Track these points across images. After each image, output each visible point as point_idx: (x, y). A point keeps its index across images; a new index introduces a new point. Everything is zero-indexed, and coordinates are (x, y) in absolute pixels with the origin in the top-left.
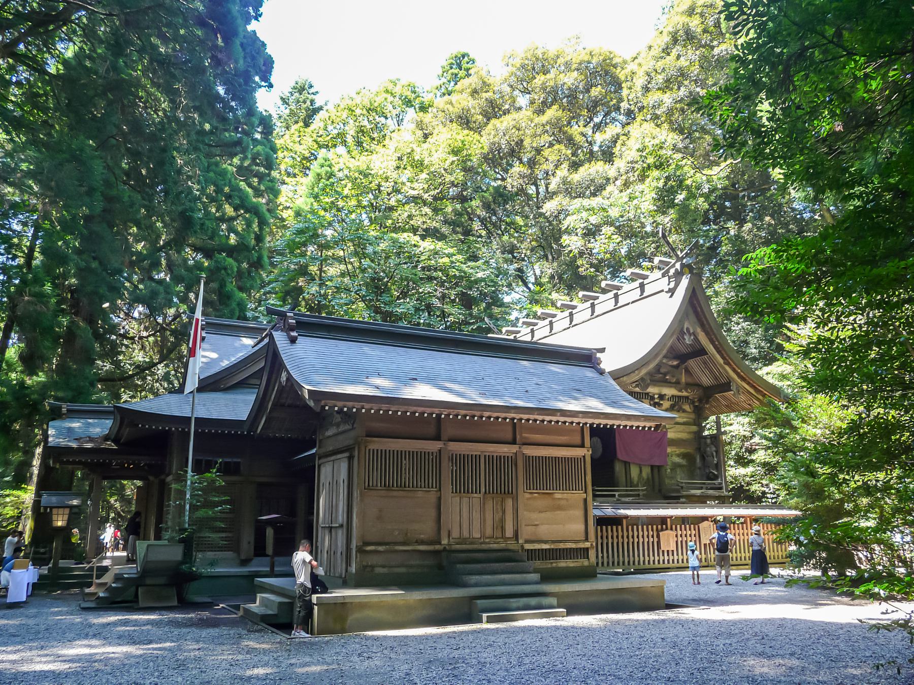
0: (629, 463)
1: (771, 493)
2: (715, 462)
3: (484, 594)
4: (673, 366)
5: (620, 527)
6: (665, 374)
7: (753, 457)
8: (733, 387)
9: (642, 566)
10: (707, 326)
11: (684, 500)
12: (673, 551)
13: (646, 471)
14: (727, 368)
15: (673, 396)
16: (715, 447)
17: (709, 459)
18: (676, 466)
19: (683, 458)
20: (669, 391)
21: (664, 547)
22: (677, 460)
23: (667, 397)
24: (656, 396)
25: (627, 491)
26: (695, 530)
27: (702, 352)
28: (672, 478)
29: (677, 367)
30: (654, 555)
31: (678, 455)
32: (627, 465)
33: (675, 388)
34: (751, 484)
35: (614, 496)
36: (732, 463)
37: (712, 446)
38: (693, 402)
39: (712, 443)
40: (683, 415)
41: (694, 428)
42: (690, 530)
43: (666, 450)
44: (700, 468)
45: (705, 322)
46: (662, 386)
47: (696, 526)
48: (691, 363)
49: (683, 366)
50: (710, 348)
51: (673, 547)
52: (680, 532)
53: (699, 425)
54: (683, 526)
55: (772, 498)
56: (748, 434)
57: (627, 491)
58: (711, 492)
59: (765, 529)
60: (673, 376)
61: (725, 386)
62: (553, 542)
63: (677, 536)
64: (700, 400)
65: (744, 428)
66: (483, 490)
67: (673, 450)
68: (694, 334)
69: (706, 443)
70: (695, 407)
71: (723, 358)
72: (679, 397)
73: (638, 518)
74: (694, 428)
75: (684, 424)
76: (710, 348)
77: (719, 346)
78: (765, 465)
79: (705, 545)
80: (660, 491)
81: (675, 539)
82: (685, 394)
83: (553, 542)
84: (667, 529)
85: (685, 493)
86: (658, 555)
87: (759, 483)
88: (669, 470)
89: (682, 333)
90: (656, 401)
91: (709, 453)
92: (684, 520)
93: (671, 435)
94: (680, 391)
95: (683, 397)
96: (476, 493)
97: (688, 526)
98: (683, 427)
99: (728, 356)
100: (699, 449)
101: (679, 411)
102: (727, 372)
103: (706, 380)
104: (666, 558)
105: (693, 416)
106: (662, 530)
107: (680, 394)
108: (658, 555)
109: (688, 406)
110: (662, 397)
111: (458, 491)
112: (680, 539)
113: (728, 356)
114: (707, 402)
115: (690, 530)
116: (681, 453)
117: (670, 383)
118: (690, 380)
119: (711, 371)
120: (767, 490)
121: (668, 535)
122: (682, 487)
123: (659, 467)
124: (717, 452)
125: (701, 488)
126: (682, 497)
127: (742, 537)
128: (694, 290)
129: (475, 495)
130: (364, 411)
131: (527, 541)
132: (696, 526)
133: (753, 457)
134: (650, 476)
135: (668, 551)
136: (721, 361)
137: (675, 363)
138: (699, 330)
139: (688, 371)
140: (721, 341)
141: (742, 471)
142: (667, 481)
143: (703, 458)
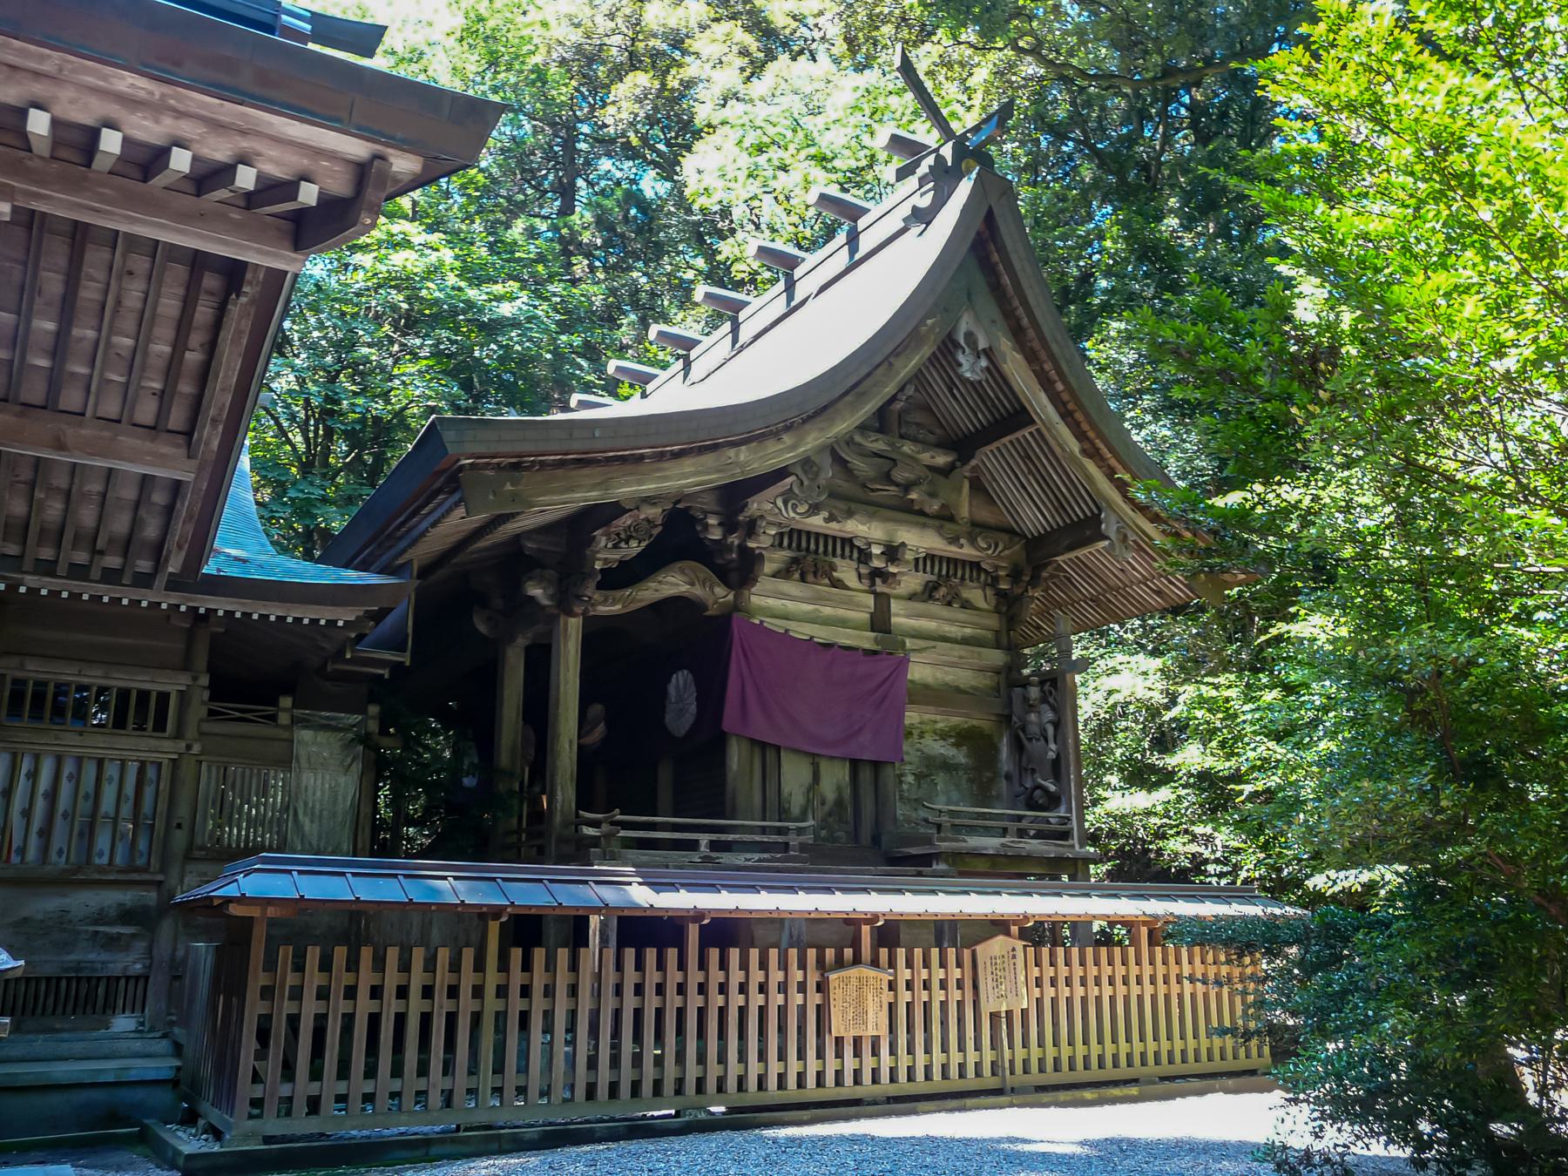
0: (778, 749)
1: (1217, 861)
2: (1052, 755)
4: (932, 469)
5: (672, 954)
6: (907, 487)
7: (1171, 761)
8: (1109, 527)
9: (752, 1095)
10: (1031, 333)
11: (942, 867)
12: (876, 1042)
13: (835, 777)
14: (1091, 466)
16: (1053, 709)
17: (1034, 747)
18: (932, 766)
19: (957, 745)
20: (918, 540)
21: (839, 1025)
22: (939, 748)
23: (909, 556)
24: (876, 550)
25: (764, 830)
26: (959, 965)
27: (1020, 416)
28: (918, 802)
29: (945, 472)
30: (801, 1055)
31: (943, 735)
32: (770, 755)
33: (939, 530)
34: (1164, 837)
35: (693, 846)
36: (1114, 779)
37: (1045, 707)
39: (1044, 700)
40: (962, 615)
41: (996, 657)
42: (1082, 963)
43: (901, 717)
44: (1008, 777)
45: (1025, 322)
47: (967, 953)
48: (987, 458)
49: (966, 471)
50: (1041, 405)
51: (875, 1024)
52: (780, 976)
53: (1012, 648)
54: (935, 952)
55: (1221, 875)
56: (1158, 698)
57: (764, 830)
58: (1033, 846)
59: (1197, 960)
60: (932, 495)
61: (1086, 529)
63: (892, 986)
64: (1015, 575)
65: (1148, 683)
67: (927, 717)
68: (988, 353)
69: (1026, 699)
70: (1001, 595)
71: (1080, 436)
72: (952, 562)
73: (776, 921)
74: (996, 657)
75: (965, 641)
76: (1041, 405)
77: (1065, 397)
78: (1205, 779)
79: (994, 1016)
80: (876, 840)
81: (887, 997)
82: (967, 551)
84: (857, 960)
85: (945, 846)
86: (820, 1055)
87: (1186, 832)
88: (910, 779)
89: (948, 347)
90: (876, 563)
91: (1034, 730)
92: (945, 932)
93: (919, 672)
94: (954, 540)
97: (951, 952)
98: (959, 650)
99: (1094, 426)
100: (1008, 718)
101: (949, 604)
102: (1089, 478)
103: (1033, 518)
104: (850, 1063)
105: (993, 622)
106: (840, 964)
107: (952, 551)
108: (820, 1055)
109: (979, 593)
112: (906, 996)
113: (1094, 426)
114: (1035, 581)
115: (1082, 963)
116: (953, 728)
117: (921, 513)
118: (985, 515)
119: (1044, 481)
120: (1207, 854)
121: (848, 980)
122: (939, 827)
123: (877, 765)
124: (1057, 725)
125: (1004, 832)
126: (937, 856)
127: (1121, 990)
128: (990, 218)
132: (967, 953)
133: (1171, 761)
134: (847, 792)
135: (857, 1041)
136: (1074, 446)
137: (942, 460)
138: (1005, 345)
139: (977, 487)
140: (1073, 381)
141: (1139, 800)
142: (901, 811)
143: (1018, 746)
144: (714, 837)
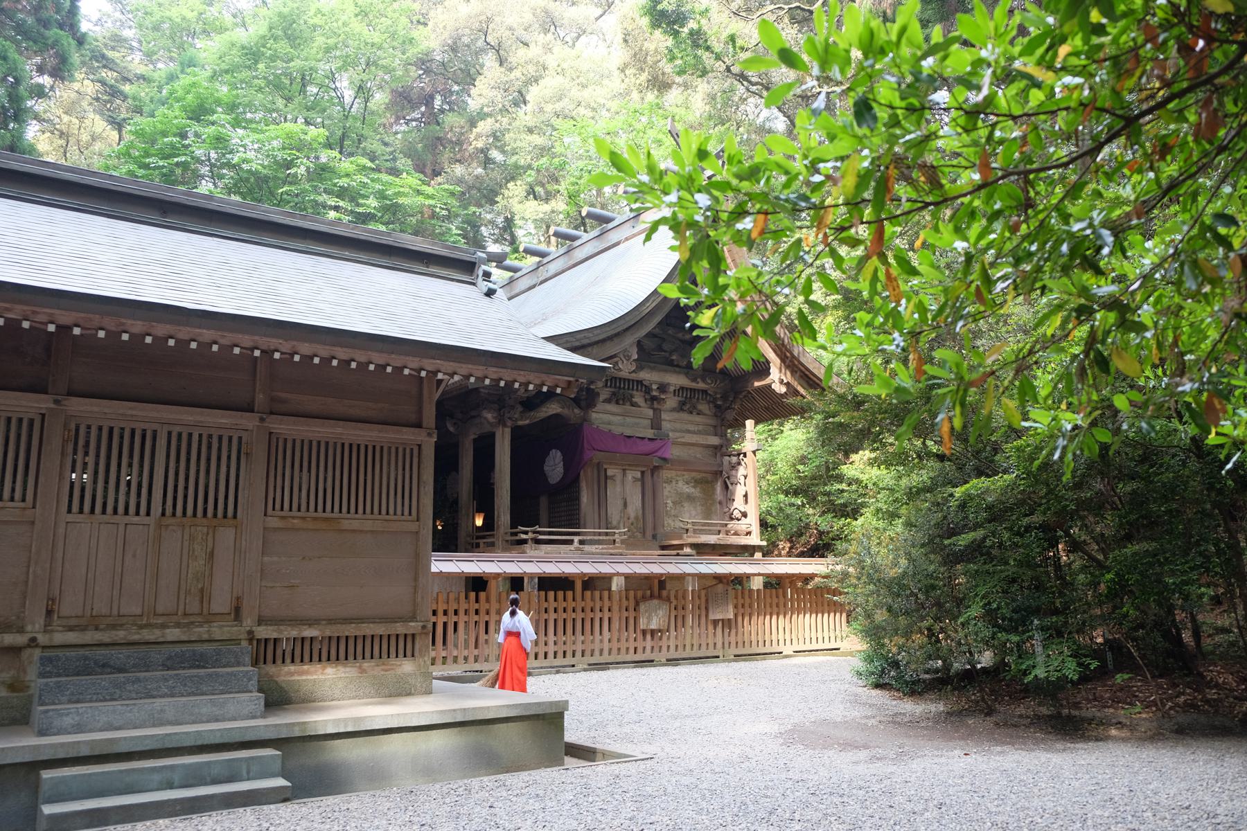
3: (229, 750)
15: (682, 388)
19: (694, 487)
23: (672, 389)
24: (655, 387)
25: (600, 534)
35: (571, 542)
38: (714, 401)
46: (666, 371)
62: (331, 621)
64: (724, 397)
66: (156, 508)
72: (693, 390)
80: (654, 537)
82: (701, 385)
83: (331, 621)
90: (655, 393)
94: (694, 380)
95: (699, 390)
96: (137, 513)
107: (694, 385)
110: (663, 388)
111: (190, 511)
129: (136, 519)
130: (237, 351)
131: (261, 621)
144: (581, 538)
